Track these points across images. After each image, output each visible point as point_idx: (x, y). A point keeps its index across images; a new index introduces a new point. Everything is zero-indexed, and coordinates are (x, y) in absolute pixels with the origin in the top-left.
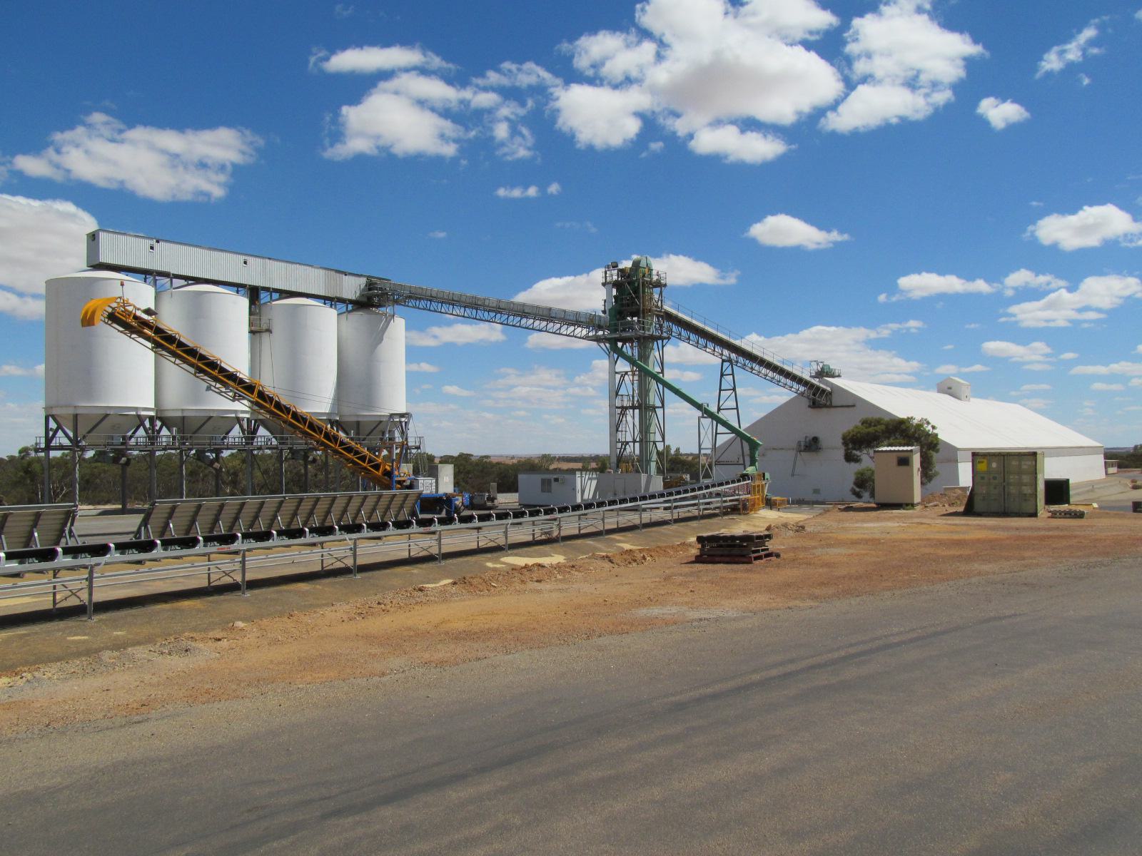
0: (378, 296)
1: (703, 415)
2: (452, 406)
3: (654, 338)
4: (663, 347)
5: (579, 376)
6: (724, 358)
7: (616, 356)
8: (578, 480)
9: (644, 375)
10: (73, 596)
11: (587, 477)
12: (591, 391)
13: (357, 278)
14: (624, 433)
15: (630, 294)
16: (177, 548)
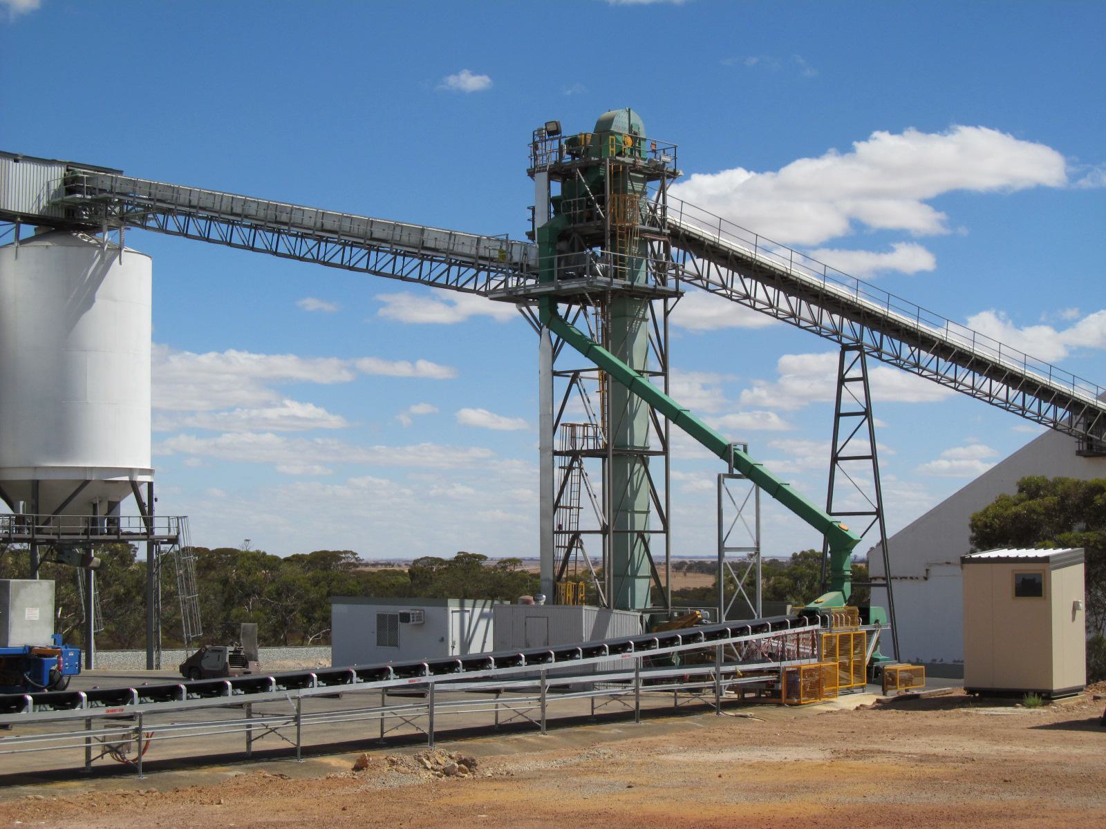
0: (85, 205)
1: (730, 470)
2: (476, 452)
3: (649, 295)
4: (666, 313)
5: (750, 387)
6: (845, 341)
7: (554, 337)
8: (454, 620)
9: (622, 388)
10: (520, 716)
11: (477, 611)
12: (774, 421)
13: (42, 169)
14: (574, 511)
15: (586, 194)
16: (49, 708)
